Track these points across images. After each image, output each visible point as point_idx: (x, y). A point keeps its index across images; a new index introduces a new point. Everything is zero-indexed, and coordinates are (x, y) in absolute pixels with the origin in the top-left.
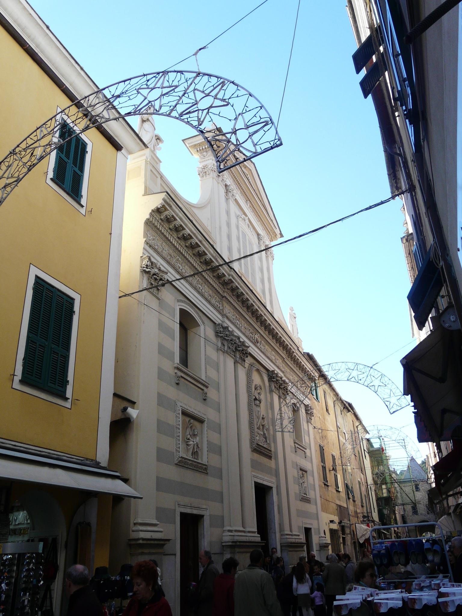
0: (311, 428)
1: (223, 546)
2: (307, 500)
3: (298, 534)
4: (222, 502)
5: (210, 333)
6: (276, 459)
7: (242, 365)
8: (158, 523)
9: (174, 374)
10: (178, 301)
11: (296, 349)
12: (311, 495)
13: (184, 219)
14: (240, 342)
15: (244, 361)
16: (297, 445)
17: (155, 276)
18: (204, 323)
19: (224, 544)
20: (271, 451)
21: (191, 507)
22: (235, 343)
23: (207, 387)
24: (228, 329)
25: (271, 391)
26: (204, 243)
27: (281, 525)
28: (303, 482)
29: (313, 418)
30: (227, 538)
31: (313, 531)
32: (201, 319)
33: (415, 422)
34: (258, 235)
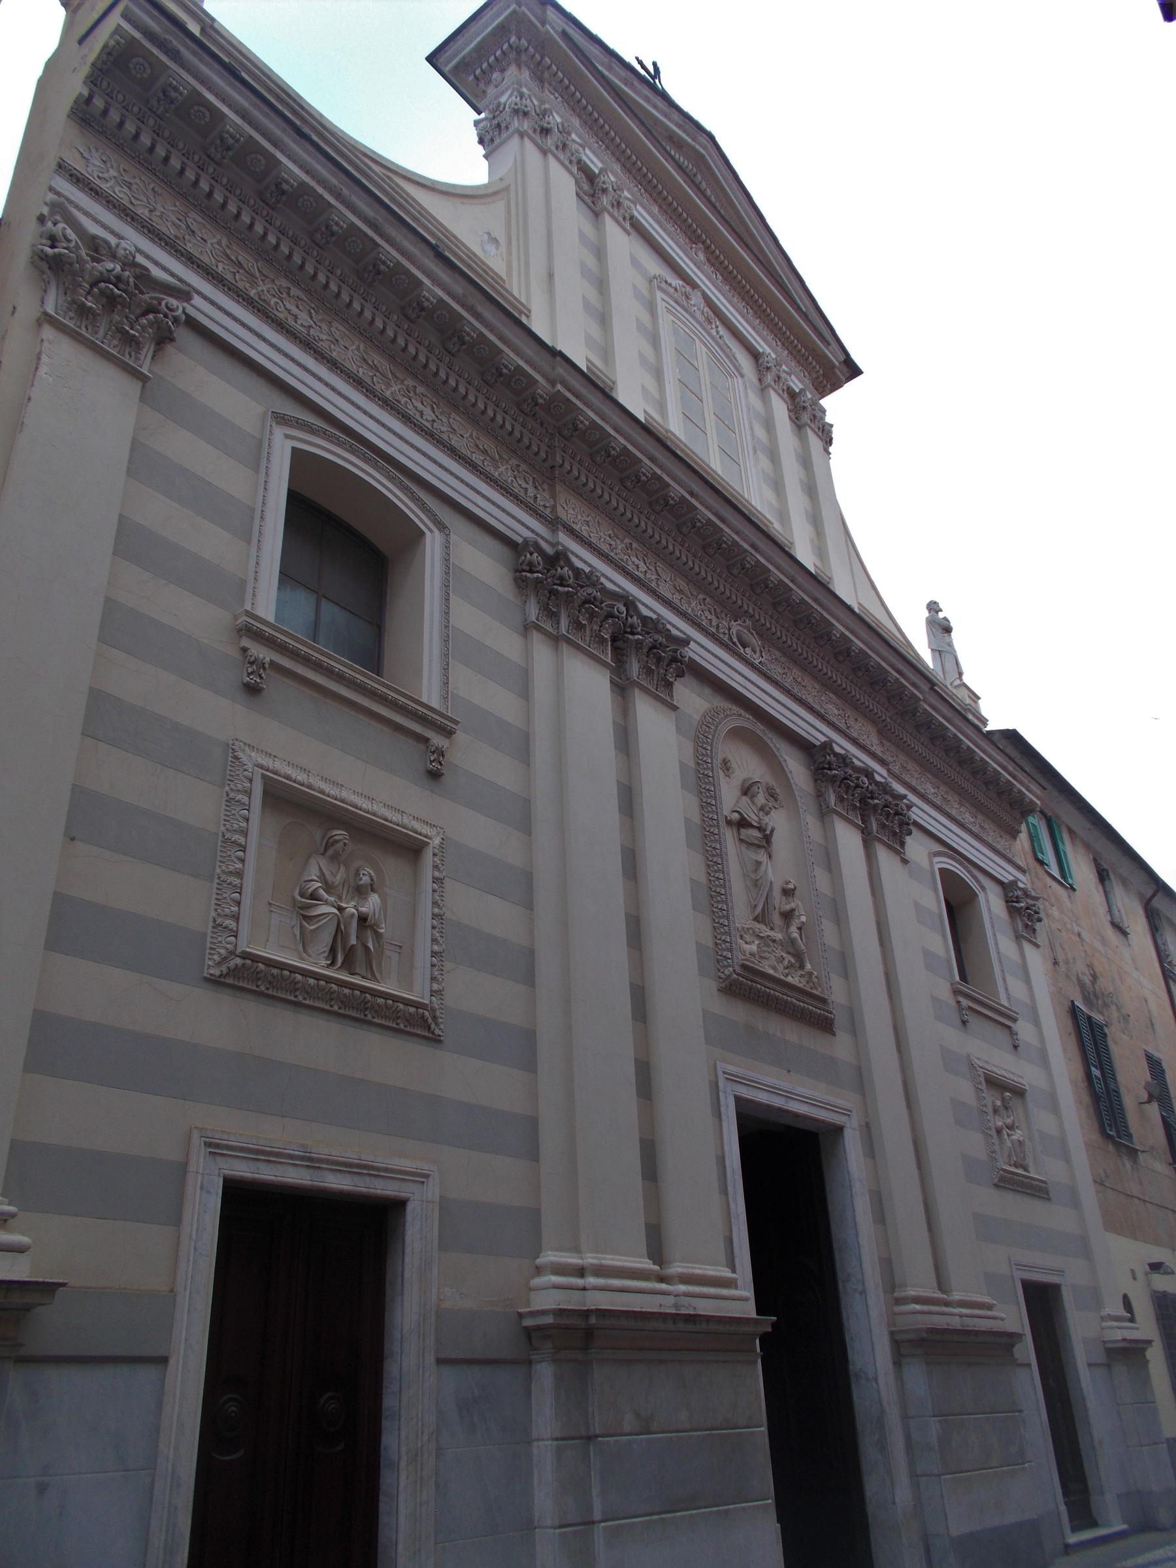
0: (1036, 960)
1: (527, 1329)
2: (1040, 1189)
3: (987, 1299)
4: (533, 1155)
5: (485, 566)
6: (855, 1029)
7: (1031, 942)
8: (12, 1209)
9: (238, 656)
10: (281, 419)
11: (925, 687)
12: (1048, 1170)
13: (257, 114)
14: (877, 783)
15: (1034, 930)
16: (965, 1002)
17: (102, 285)
18: (442, 527)
19: (528, 1322)
20: (824, 1001)
21: (311, 1162)
22: (858, 786)
23: (449, 733)
24: (832, 748)
25: (824, 813)
26: (392, 232)
27: (887, 1264)
28: (1011, 1127)
29: (1038, 926)
30: (548, 1296)
31: (1067, 1296)
32: (978, 881)
33: (648, 81)
34: (756, 356)
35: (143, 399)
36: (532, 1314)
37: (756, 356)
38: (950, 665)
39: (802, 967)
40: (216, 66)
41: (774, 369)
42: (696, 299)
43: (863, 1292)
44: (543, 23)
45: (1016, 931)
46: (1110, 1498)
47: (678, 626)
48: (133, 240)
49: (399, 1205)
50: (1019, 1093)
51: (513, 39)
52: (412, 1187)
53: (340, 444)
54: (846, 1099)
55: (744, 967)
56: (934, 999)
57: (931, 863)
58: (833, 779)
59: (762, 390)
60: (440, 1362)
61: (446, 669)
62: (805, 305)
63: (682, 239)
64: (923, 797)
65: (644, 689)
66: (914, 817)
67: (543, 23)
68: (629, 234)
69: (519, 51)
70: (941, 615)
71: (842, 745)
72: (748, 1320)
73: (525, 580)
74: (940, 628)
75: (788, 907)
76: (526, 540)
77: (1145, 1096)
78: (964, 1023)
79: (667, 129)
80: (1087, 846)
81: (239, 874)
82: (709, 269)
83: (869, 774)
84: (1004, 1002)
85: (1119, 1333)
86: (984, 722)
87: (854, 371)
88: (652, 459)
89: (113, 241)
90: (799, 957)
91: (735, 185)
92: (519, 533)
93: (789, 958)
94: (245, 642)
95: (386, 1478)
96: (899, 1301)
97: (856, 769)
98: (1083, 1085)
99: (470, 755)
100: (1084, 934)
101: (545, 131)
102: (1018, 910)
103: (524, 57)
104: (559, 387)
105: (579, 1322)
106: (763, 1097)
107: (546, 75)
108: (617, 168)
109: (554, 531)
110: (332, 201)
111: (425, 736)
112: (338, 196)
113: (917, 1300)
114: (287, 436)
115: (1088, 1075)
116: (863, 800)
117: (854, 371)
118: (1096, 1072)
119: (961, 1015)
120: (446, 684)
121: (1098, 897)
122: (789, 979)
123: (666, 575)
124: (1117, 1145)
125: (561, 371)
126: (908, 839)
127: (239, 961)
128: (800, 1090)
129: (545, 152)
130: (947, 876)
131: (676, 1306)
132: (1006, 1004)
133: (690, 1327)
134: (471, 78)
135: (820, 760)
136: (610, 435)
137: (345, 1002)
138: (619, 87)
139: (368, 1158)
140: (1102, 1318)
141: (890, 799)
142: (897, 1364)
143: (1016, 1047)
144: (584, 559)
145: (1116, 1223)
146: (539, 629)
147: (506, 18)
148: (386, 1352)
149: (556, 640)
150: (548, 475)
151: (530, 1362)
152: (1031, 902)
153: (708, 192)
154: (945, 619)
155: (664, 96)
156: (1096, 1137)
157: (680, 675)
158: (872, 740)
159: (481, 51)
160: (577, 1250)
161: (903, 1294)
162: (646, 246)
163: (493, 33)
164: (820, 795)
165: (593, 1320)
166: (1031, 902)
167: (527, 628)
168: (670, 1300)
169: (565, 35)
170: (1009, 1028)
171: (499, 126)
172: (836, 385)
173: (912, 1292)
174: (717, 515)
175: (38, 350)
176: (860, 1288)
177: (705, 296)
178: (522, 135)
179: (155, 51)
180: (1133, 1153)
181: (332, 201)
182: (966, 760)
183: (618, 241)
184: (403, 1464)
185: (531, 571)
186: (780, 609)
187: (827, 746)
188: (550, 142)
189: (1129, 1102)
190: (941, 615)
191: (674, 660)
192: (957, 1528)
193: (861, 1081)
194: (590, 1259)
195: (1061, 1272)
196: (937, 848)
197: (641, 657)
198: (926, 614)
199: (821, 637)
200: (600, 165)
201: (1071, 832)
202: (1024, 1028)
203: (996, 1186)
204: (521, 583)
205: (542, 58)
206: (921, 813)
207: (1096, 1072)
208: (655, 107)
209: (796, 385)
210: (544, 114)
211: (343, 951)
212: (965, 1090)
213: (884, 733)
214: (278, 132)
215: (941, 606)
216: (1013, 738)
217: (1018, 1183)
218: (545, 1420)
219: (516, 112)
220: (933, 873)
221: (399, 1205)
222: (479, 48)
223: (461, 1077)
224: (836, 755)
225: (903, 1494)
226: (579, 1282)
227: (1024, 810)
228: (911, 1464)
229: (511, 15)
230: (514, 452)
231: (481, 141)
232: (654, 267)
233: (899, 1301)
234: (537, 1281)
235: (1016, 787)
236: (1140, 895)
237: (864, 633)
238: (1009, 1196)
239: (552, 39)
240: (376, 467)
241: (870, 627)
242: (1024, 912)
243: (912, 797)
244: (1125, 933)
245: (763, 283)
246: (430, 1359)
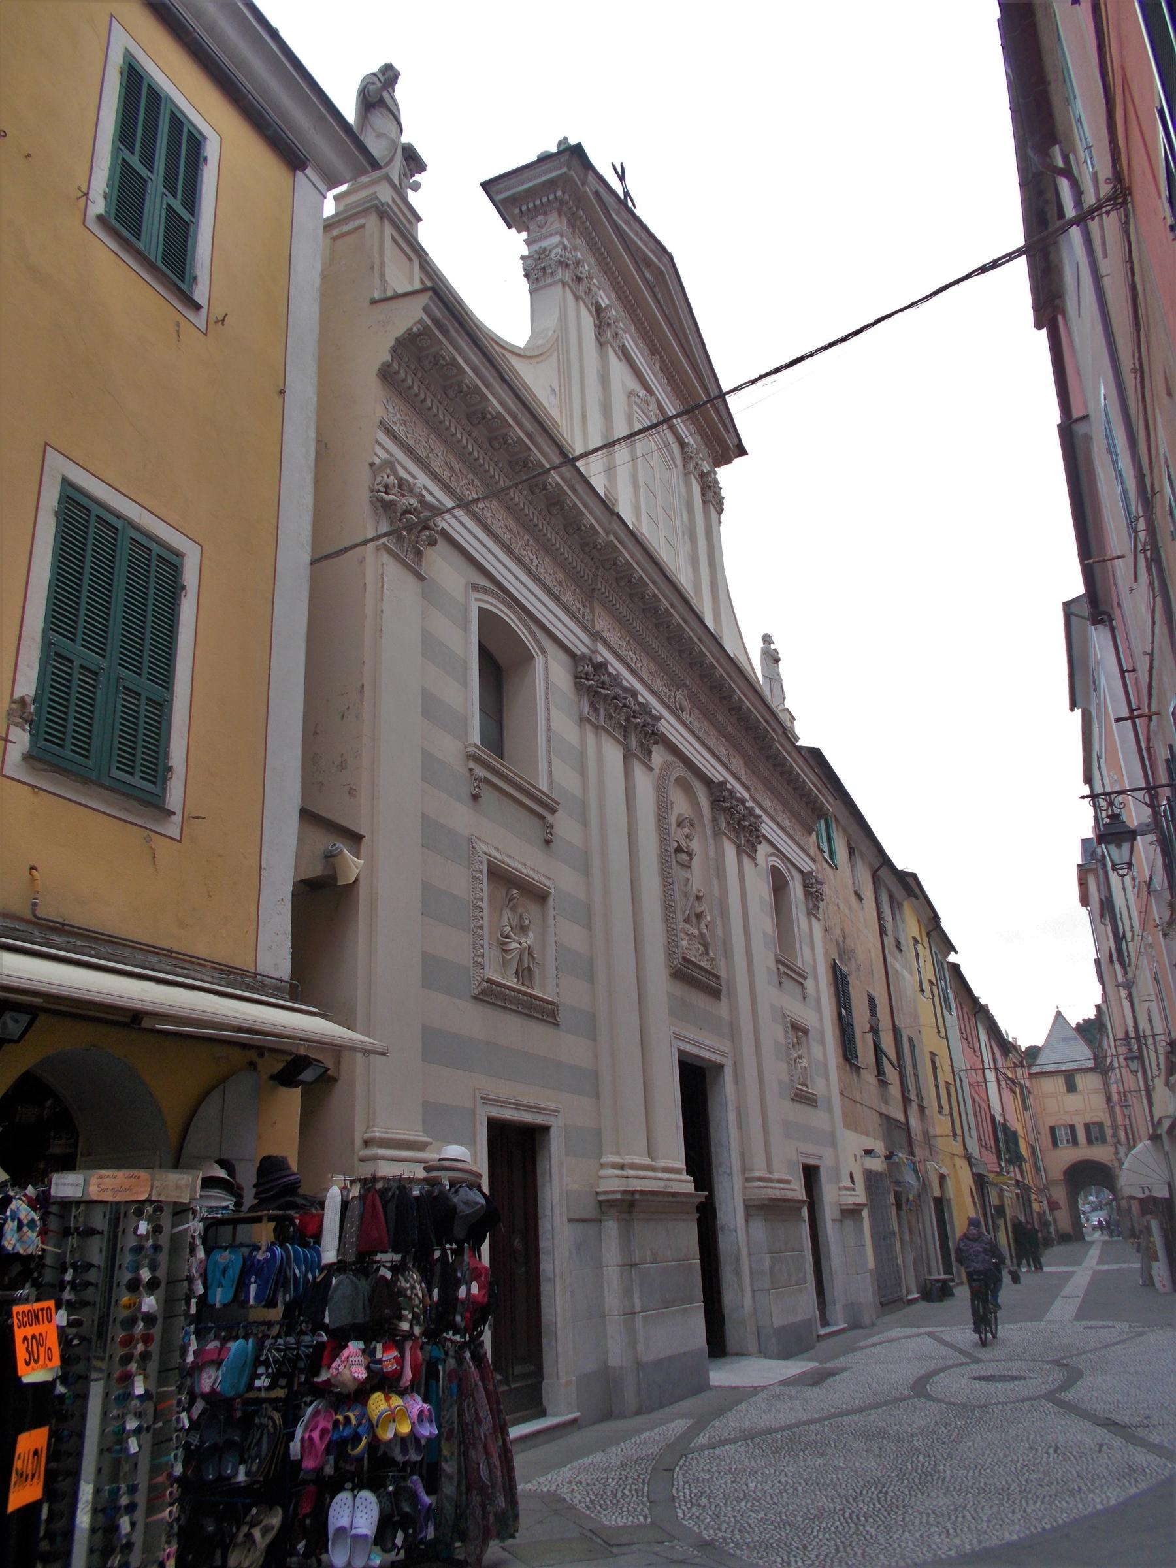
0: (817, 927)
1: (601, 1203)
8: (429, 1140)
10: (476, 588)
11: (780, 731)
12: (818, 1087)
14: (640, 704)
16: (783, 969)
19: (602, 1197)
20: (718, 977)
21: (517, 1106)
22: (625, 706)
25: (717, 833)
28: (800, 1057)
29: (821, 904)
30: (612, 1184)
34: (682, 444)
35: (425, 596)
36: (606, 1193)
37: (682, 444)
38: (776, 692)
39: (707, 954)
40: (466, 337)
41: (613, 326)
42: (653, 406)
43: (731, 1174)
44: (584, 184)
45: (808, 909)
46: (839, 1306)
47: (657, 707)
48: (422, 480)
49: (546, 1129)
50: (540, 896)
51: (559, 193)
52: (553, 1119)
53: (503, 602)
54: (725, 1046)
55: (684, 958)
56: (768, 968)
57: (467, 597)
58: (724, 809)
59: (685, 474)
60: (570, 1220)
61: (550, 763)
62: (725, 415)
63: (647, 353)
64: (772, 819)
65: (639, 758)
66: (662, 729)
67: (584, 184)
68: (620, 360)
69: (562, 202)
70: (773, 647)
71: (732, 783)
72: (690, 1195)
73: (581, 684)
74: (772, 658)
75: (700, 910)
76: (583, 654)
77: (867, 1029)
78: (475, 797)
79: (644, 253)
80: (845, 831)
81: (481, 927)
82: (661, 375)
83: (634, 694)
84: (543, 785)
85: (849, 1200)
86: (797, 739)
87: (742, 451)
88: (654, 583)
89: (410, 479)
90: (706, 945)
91: (681, 298)
92: (580, 649)
93: (702, 948)
94: (472, 765)
95: (545, 1288)
96: (748, 1180)
97: (626, 690)
98: (836, 1022)
99: (565, 826)
100: (841, 905)
101: (579, 279)
102: (811, 893)
103: (565, 208)
104: (612, 537)
105: (629, 1197)
106: (695, 1050)
107: (578, 223)
108: (592, 260)
109: (594, 641)
110: (510, 421)
111: (539, 808)
112: (514, 418)
113: (760, 1179)
114: (476, 600)
115: (839, 1014)
116: (627, 720)
117: (742, 451)
118: (844, 1012)
119: (780, 978)
120: (550, 774)
121: (848, 873)
122: (702, 964)
123: (439, 449)
124: (851, 1064)
125: (616, 526)
126: (759, 847)
127: (485, 984)
128: (707, 1042)
129: (577, 298)
130: (774, 868)
131: (666, 1187)
132: (545, 790)
133: (674, 1199)
134: (517, 211)
135: (719, 795)
136: (510, 425)
137: (518, 1002)
138: (629, 236)
139: (538, 1102)
140: (840, 1189)
141: (649, 720)
142: (747, 1221)
143: (548, 842)
144: (616, 666)
145: (851, 1123)
146: (589, 721)
147: (557, 177)
148: (540, 1215)
149: (597, 727)
150: (590, 595)
151: (601, 1221)
152: (753, 820)
153: (659, 296)
154: (775, 650)
155: (638, 220)
156: (841, 1060)
157: (656, 743)
158: (742, 772)
159: (530, 194)
160: (618, 1153)
161: (752, 1175)
162: (630, 370)
163: (543, 184)
164: (714, 820)
165: (637, 1196)
166: (753, 820)
167: (582, 720)
168: (662, 1183)
169: (597, 194)
170: (543, 818)
171: (544, 269)
172: (728, 460)
173: (757, 1174)
174: (684, 619)
175: (380, 572)
176: (728, 1171)
177: (658, 401)
178: (564, 284)
179: (437, 332)
180: (858, 1069)
181: (510, 421)
182: (777, 764)
183: (617, 368)
184: (557, 1279)
185: (587, 679)
186: (622, 584)
187: (723, 784)
188: (581, 289)
189: (858, 1032)
190: (773, 647)
191: (653, 733)
192: (778, 1322)
193: (733, 1033)
194: (627, 1159)
195: (820, 1157)
196: (772, 850)
197: (637, 732)
198: (761, 644)
199: (725, 698)
200: (607, 302)
201: (836, 820)
202: (809, 984)
203: (475, 998)
204: (578, 687)
205: (577, 209)
206: (768, 828)
207: (844, 1012)
208: (641, 239)
209: (604, 302)
210: (578, 263)
211: (525, 973)
212: (460, 882)
213: (748, 764)
214: (491, 379)
215: (774, 639)
216: (816, 756)
217: (804, 1098)
218: (612, 1252)
219: (560, 263)
220: (466, 610)
221: (546, 1129)
222: (528, 191)
223: (569, 1047)
224: (609, 674)
225: (748, 1302)
226: (624, 1173)
227: (819, 813)
228: (752, 1285)
229: (561, 175)
230: (528, 530)
231: (527, 276)
232: (633, 384)
233: (748, 1180)
234: (603, 1173)
235: (815, 793)
236: (871, 865)
237: (631, 544)
238: (798, 1106)
239: (588, 196)
240: (514, 612)
241: (756, 691)
242: (813, 891)
243: (765, 818)
244: (861, 899)
245: (612, 242)
246: (565, 1220)
